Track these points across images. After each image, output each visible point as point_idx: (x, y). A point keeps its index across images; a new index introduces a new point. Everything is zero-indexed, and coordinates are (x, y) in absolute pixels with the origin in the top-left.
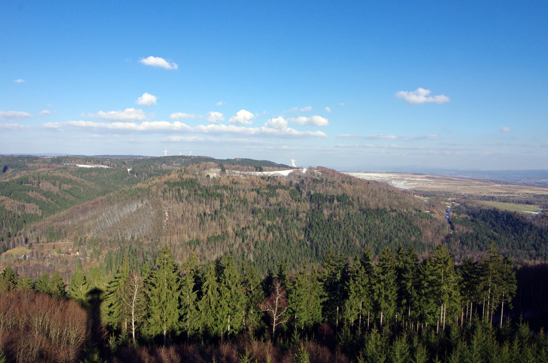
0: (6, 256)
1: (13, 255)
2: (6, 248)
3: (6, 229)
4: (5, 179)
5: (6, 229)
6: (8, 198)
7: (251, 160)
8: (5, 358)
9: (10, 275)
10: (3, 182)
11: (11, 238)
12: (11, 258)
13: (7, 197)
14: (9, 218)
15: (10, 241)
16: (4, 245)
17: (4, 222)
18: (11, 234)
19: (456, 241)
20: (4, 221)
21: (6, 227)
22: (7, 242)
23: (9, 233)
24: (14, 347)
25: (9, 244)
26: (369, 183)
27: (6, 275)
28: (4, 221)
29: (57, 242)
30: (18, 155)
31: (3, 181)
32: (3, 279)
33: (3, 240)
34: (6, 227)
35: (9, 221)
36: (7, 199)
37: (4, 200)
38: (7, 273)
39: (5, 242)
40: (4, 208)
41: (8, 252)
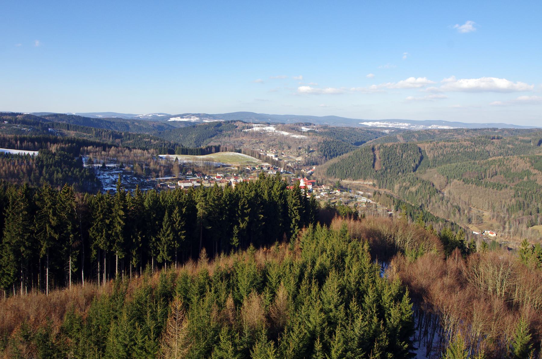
0: (533, 231)
1: (540, 231)
2: (533, 222)
3: (536, 203)
4: (539, 153)
5: (536, 203)
6: (541, 173)
7: (65, 115)
8: (531, 337)
9: (538, 252)
10: (537, 156)
11: (540, 214)
12: (538, 235)
13: (539, 171)
14: (540, 193)
15: (538, 216)
16: (531, 220)
17: (534, 196)
18: (539, 209)
19: (198, 182)
20: (534, 195)
21: (536, 202)
22: (535, 217)
23: (538, 208)
24: (539, 329)
25: (536, 220)
26: (194, 127)
27: (535, 251)
28: (534, 195)
29: (254, 182)
30: (332, 125)
31: (537, 155)
32: (531, 254)
33: (531, 214)
34: (536, 202)
35: (539, 196)
36: (539, 173)
37: (536, 174)
38: (536, 249)
39: (533, 217)
40: (536, 182)
41: (535, 227)
